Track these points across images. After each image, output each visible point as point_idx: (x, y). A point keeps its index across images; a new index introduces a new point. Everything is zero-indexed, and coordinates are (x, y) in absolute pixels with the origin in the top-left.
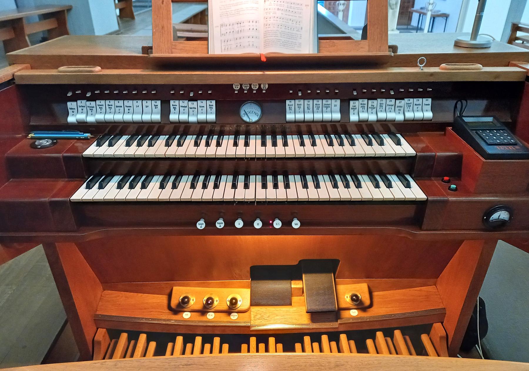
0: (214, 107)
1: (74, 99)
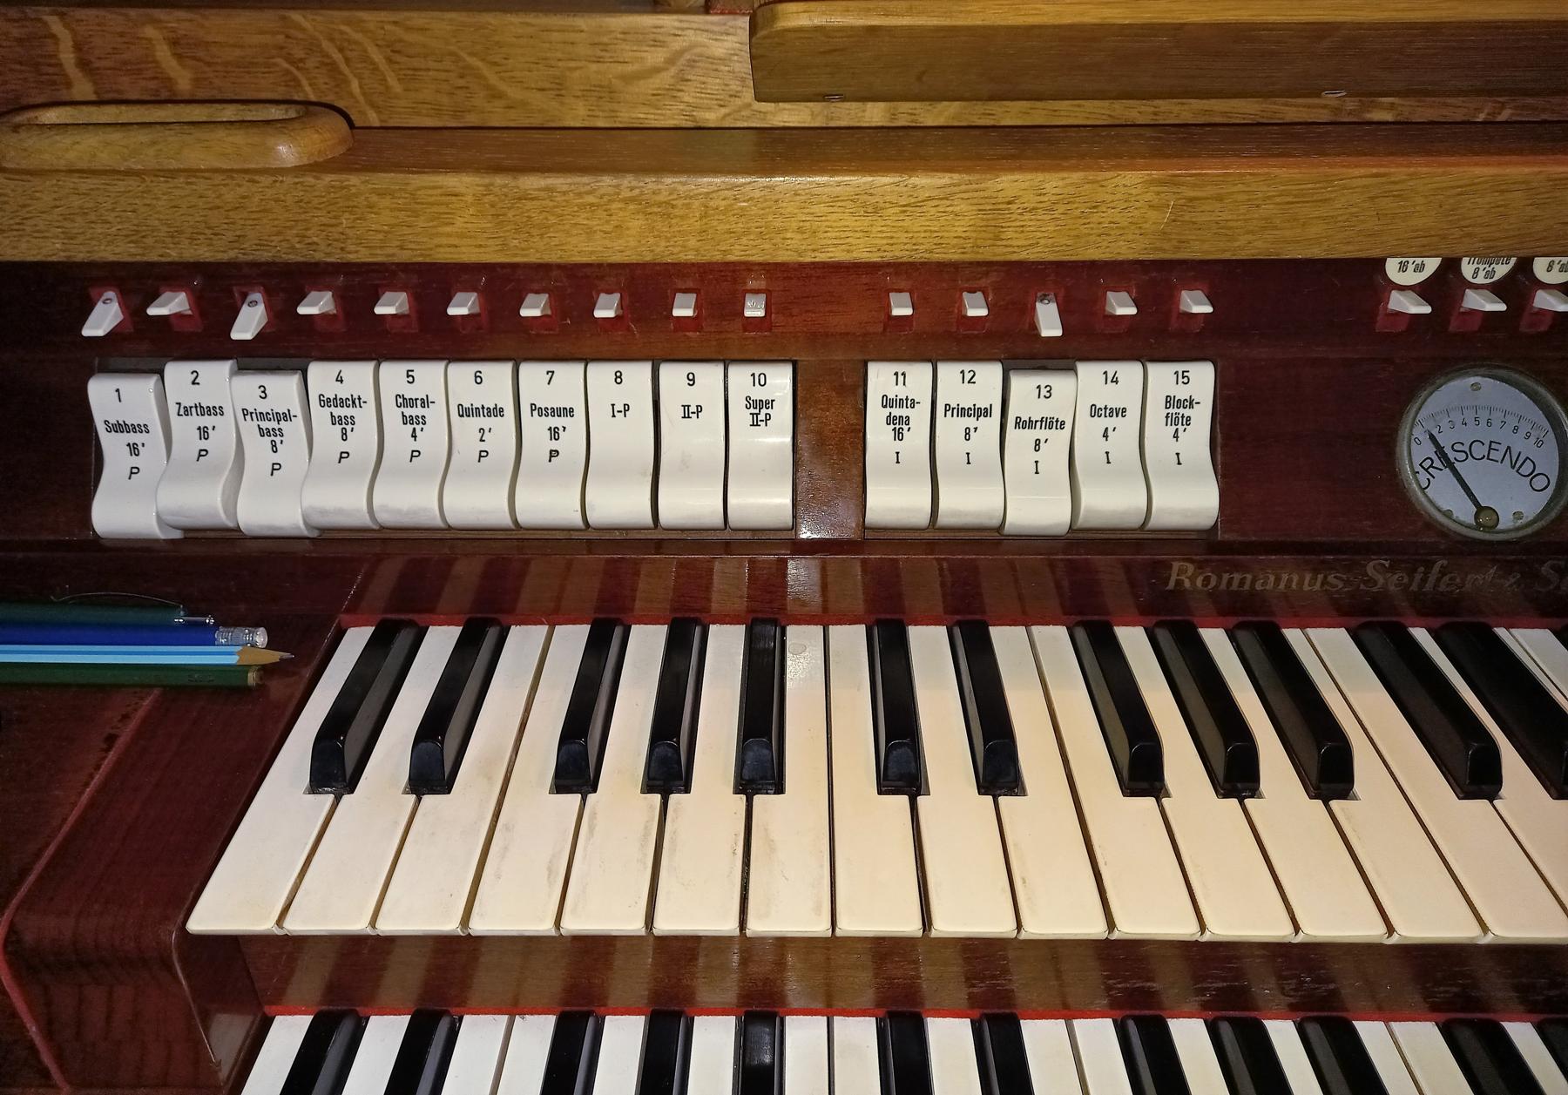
0: (783, 412)
1: (144, 347)
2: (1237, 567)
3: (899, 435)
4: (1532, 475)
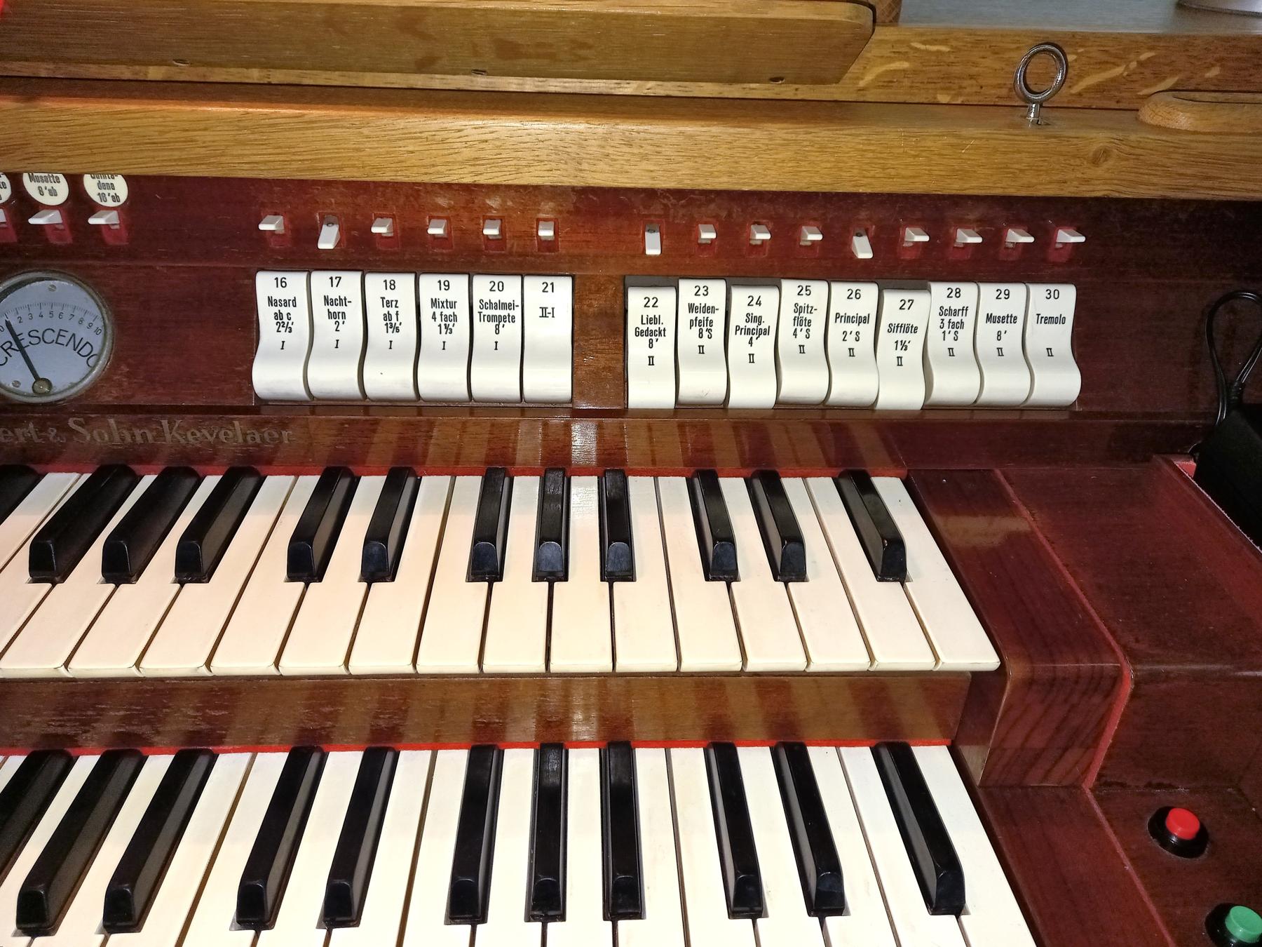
1: (299, 255)
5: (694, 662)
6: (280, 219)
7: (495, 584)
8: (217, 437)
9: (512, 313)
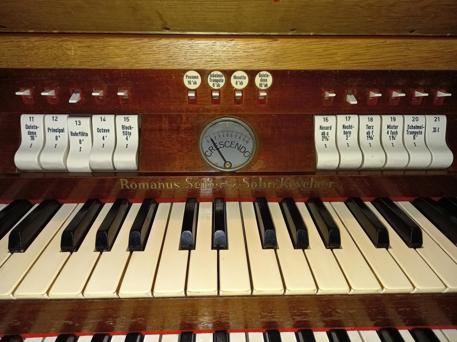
2: (156, 181)
3: (33, 138)
4: (244, 152)
5: (292, 290)
6: (53, 91)
7: (192, 251)
8: (302, 185)
9: (421, 130)
